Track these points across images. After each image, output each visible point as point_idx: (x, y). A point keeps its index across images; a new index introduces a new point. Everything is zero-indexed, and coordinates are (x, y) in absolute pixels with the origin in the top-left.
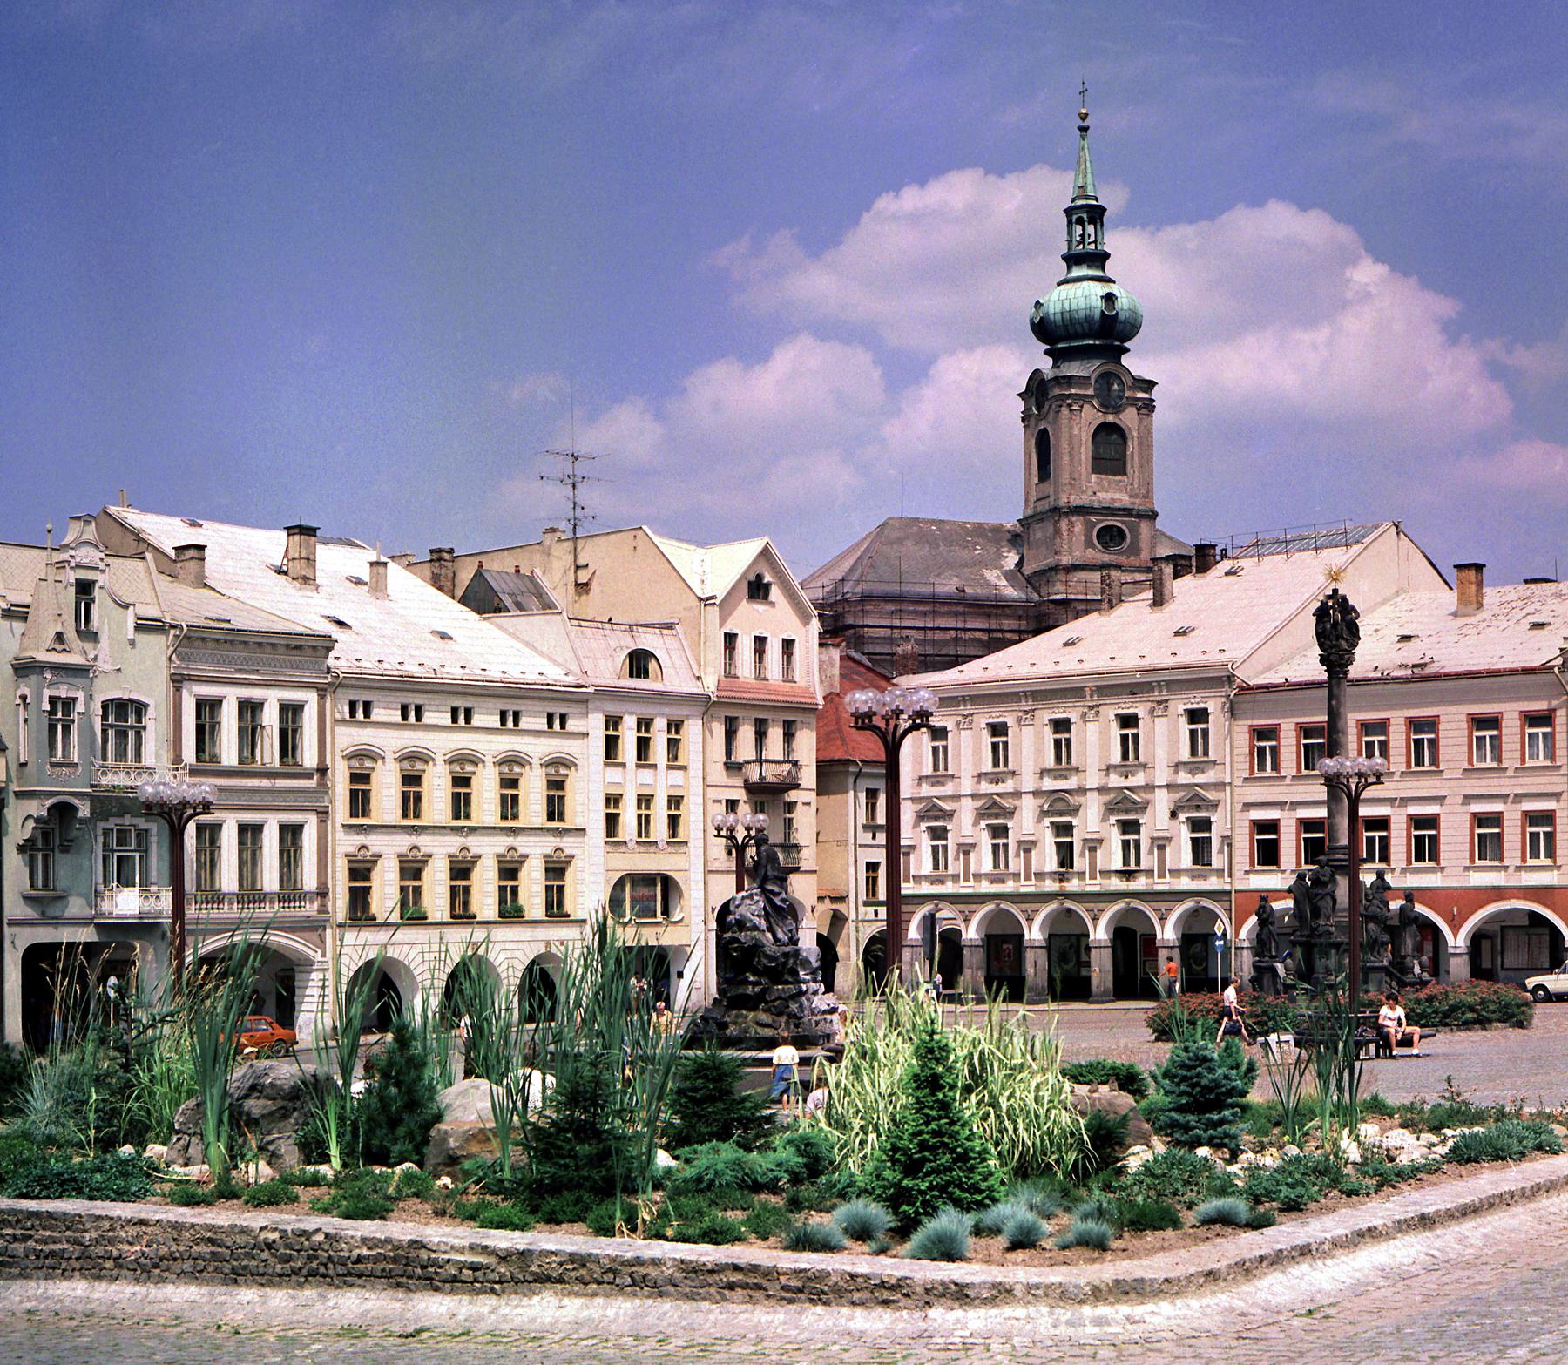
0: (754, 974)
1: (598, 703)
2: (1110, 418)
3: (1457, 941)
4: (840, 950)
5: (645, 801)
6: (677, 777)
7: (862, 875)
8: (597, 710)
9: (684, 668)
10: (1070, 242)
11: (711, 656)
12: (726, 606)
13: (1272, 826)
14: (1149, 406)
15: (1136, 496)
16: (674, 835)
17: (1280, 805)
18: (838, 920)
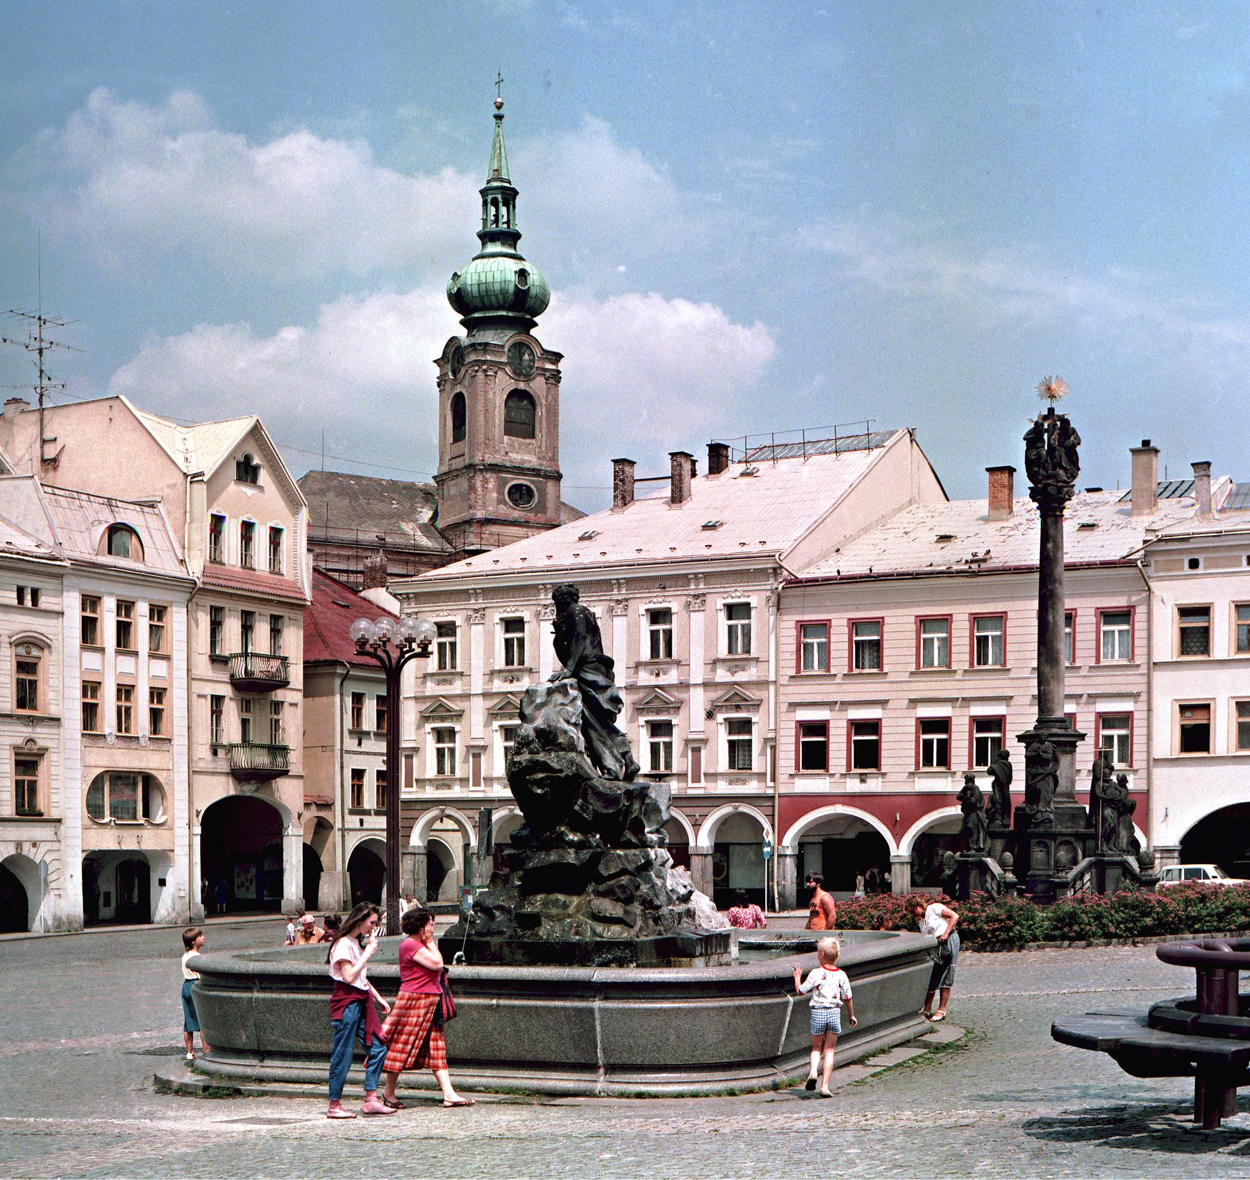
0: (574, 830)
1: (75, 580)
2: (522, 386)
3: (901, 849)
4: (325, 859)
5: (125, 691)
6: (160, 667)
7: (348, 782)
8: (73, 588)
9: (170, 549)
10: (485, 221)
11: (196, 538)
12: (214, 484)
13: (820, 728)
14: (556, 377)
15: (543, 458)
16: (155, 731)
17: (831, 705)
18: (322, 827)
